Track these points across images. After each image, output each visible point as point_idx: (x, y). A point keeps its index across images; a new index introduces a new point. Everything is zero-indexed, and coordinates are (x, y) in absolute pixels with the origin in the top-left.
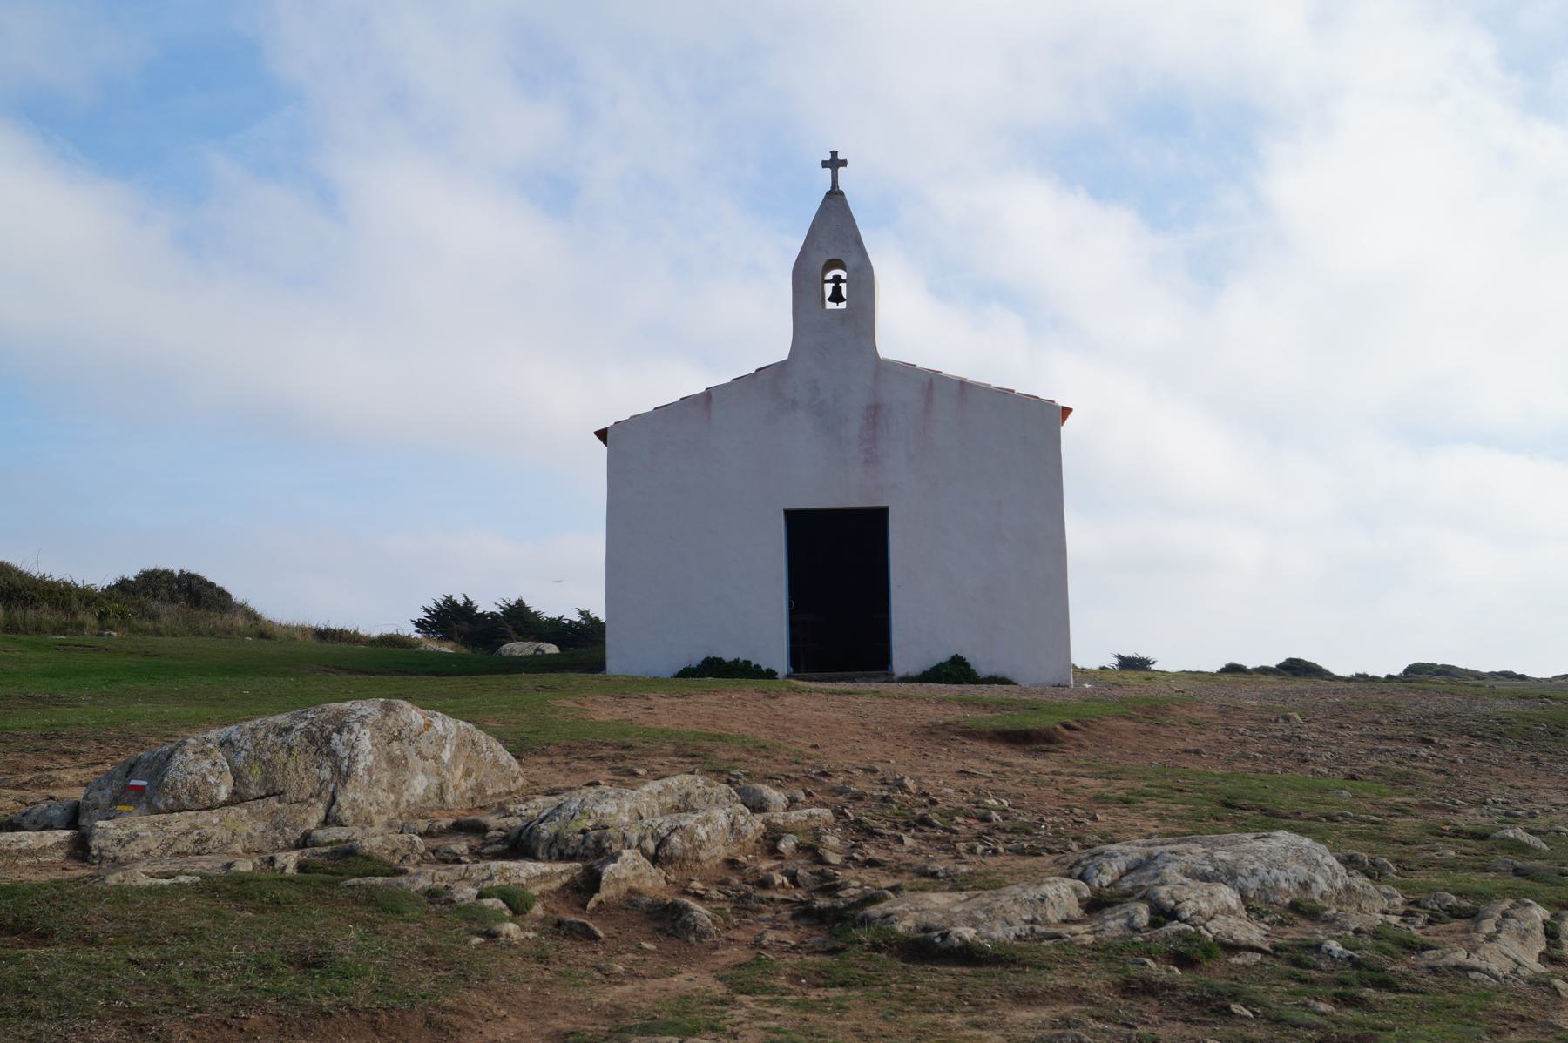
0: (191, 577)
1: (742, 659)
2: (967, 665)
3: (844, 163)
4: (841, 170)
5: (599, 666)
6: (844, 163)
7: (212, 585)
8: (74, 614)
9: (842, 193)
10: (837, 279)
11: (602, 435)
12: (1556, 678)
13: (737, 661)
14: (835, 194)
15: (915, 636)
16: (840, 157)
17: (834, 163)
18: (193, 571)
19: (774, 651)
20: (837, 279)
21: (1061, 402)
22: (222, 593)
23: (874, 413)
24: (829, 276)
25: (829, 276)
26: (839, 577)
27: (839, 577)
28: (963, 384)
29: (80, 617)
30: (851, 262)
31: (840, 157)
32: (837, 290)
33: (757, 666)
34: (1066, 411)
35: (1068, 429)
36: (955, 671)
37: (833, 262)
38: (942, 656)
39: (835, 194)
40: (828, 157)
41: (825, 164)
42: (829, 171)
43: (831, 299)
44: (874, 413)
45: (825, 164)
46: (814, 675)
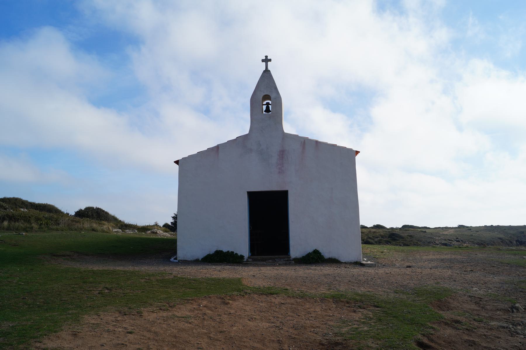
0: (98, 209)
1: (230, 251)
2: (320, 253)
3: (270, 60)
4: (269, 63)
5: (174, 252)
6: (270, 60)
7: (104, 211)
8: (31, 224)
9: (269, 71)
10: (268, 104)
11: (177, 162)
12: (436, 228)
13: (228, 251)
14: (267, 72)
15: (299, 244)
16: (269, 58)
17: (266, 60)
18: (99, 207)
19: (243, 248)
20: (268, 104)
21: (355, 149)
22: (107, 213)
23: (282, 154)
24: (265, 103)
25: (265, 103)
26: (269, 213)
27: (269, 213)
28: (317, 142)
29: (33, 225)
30: (273, 96)
31: (269, 58)
32: (268, 108)
33: (236, 254)
34: (357, 152)
35: (358, 158)
36: (314, 258)
37: (266, 99)
38: (310, 250)
39: (267, 72)
40: (264, 58)
41: (263, 61)
42: (264, 63)
43: (265, 111)
44: (282, 154)
45: (263, 61)
46: (259, 257)
